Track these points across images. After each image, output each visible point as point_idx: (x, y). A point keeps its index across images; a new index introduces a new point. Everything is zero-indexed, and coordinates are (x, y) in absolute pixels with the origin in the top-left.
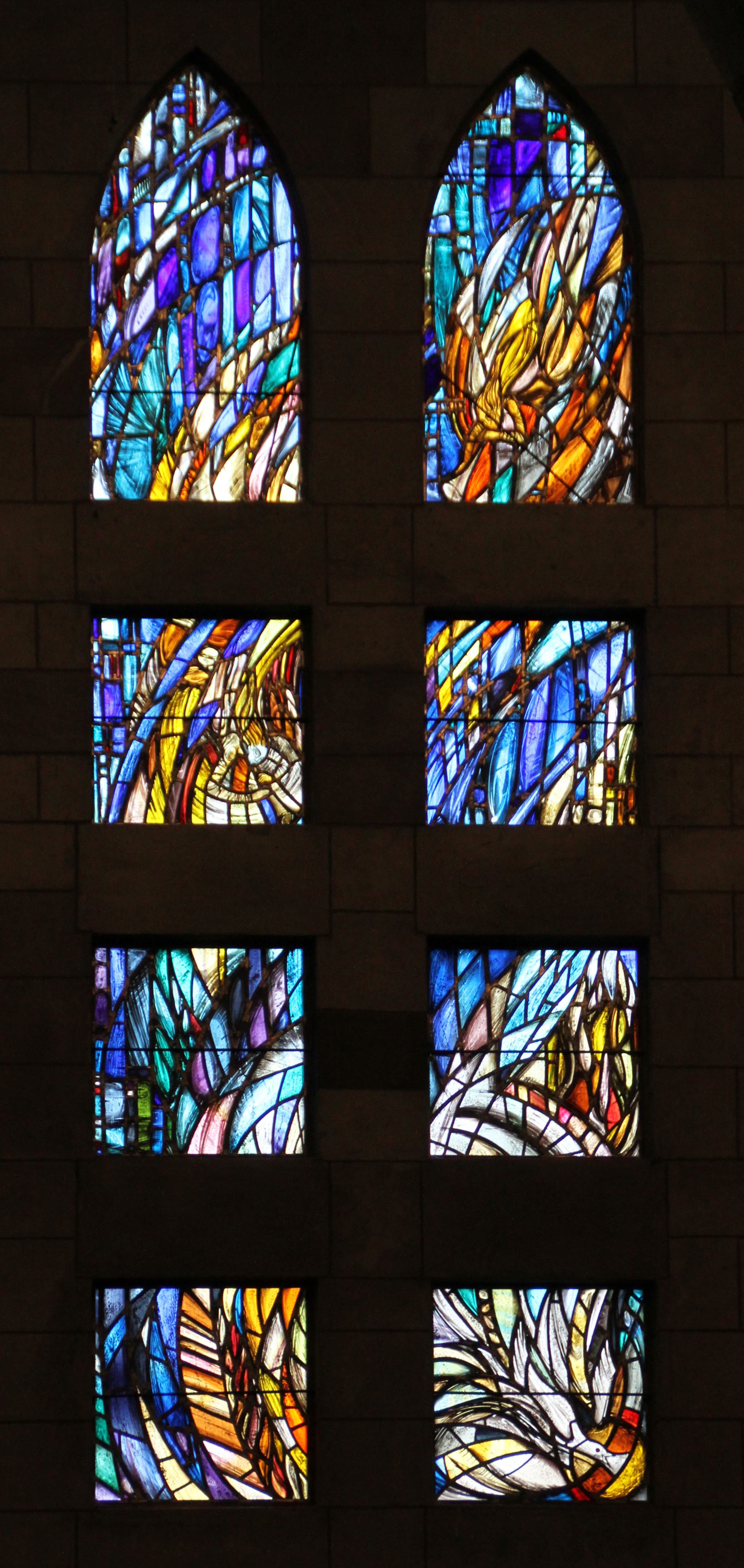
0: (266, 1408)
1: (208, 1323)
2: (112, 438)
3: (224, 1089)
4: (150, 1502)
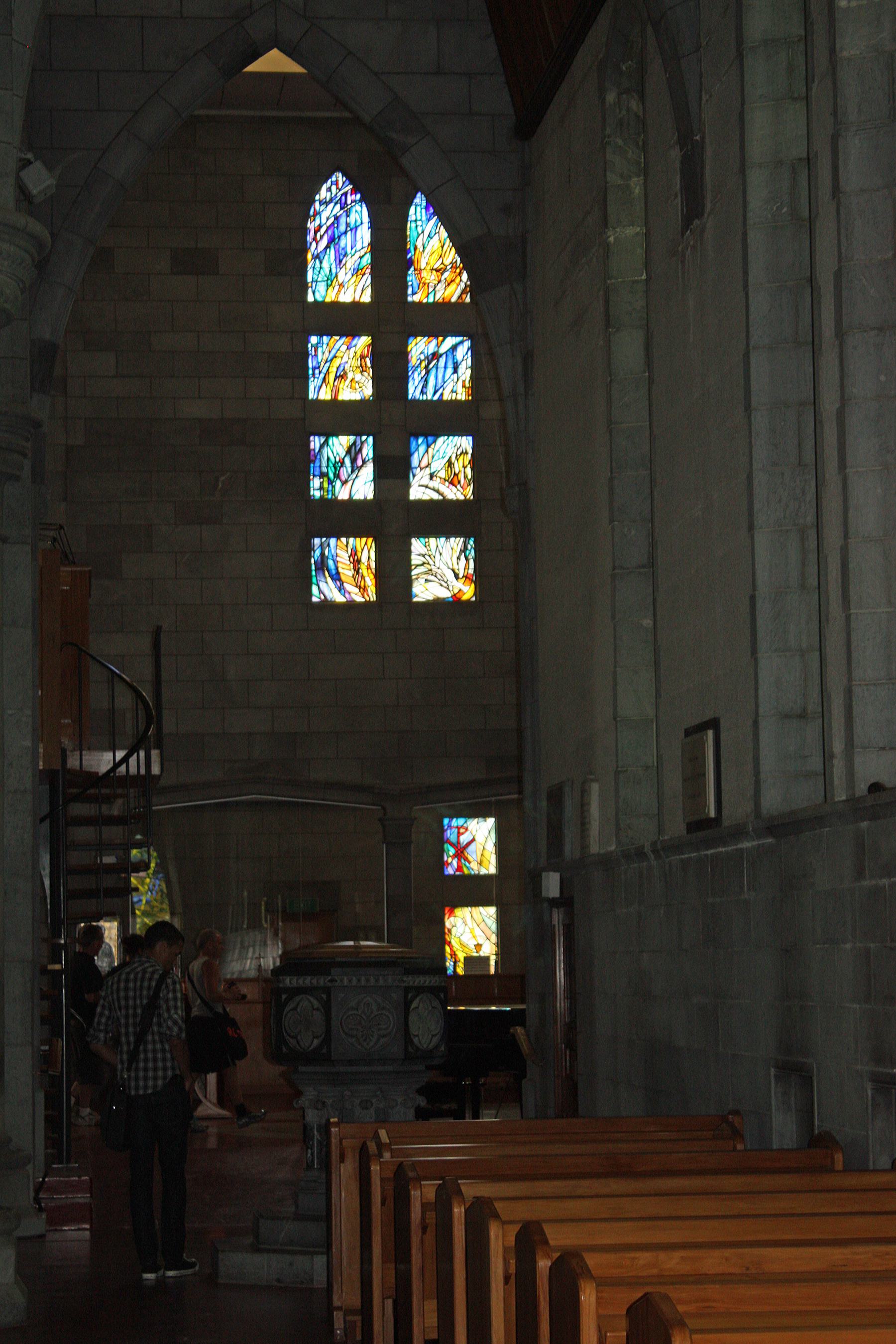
3: (349, 479)
4: (328, 602)
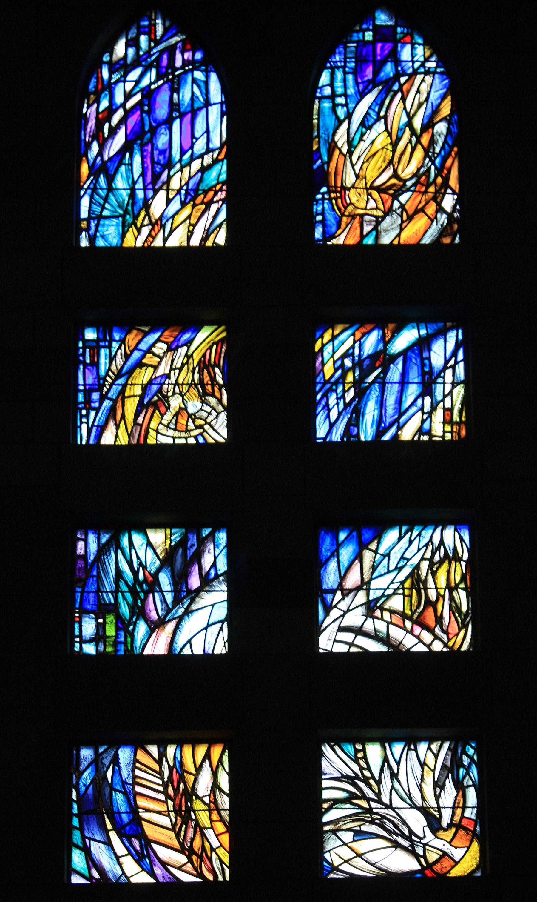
0: (198, 822)
1: (156, 767)
2: (94, 219)
